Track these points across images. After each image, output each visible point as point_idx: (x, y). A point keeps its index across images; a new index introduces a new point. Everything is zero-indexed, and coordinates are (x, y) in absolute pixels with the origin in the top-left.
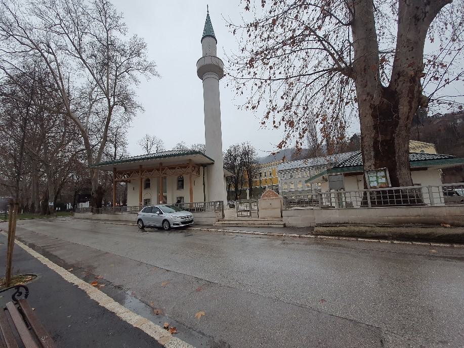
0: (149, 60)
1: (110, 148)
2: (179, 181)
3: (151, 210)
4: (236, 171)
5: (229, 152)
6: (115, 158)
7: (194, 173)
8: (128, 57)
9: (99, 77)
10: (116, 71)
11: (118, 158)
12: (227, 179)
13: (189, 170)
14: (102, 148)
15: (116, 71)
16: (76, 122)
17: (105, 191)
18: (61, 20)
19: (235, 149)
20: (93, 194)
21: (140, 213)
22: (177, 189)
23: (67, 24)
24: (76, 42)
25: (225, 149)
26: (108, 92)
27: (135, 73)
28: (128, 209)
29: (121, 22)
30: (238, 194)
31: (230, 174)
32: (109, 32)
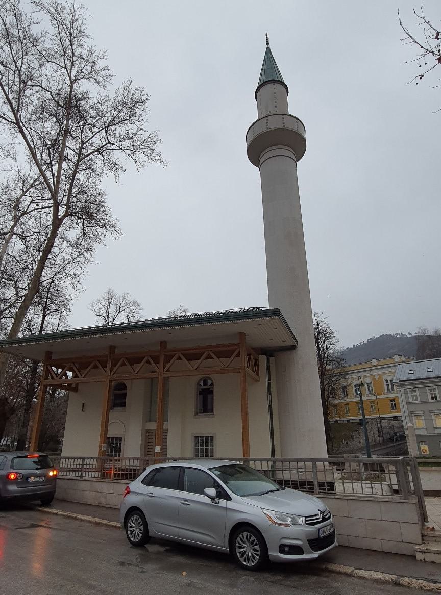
1: (34, 315)
21: (136, 485)
22: (196, 414)
27: (118, 156)
29: (101, 64)
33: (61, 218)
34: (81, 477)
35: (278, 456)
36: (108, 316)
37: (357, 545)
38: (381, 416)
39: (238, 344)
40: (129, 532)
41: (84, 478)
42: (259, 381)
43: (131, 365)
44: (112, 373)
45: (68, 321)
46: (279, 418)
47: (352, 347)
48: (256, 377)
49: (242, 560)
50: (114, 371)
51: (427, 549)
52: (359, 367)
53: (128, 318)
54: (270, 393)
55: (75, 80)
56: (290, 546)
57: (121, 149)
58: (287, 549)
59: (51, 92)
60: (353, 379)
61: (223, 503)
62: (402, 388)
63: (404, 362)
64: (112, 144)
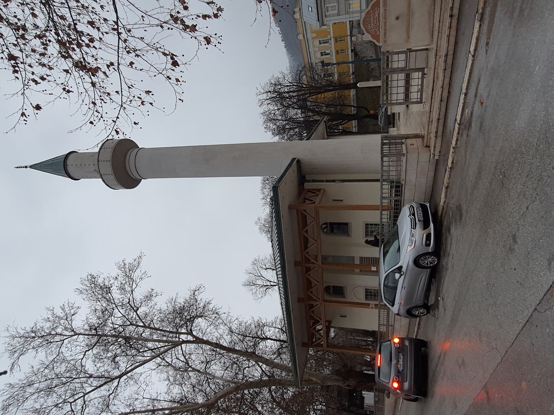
0: (115, 272)
2: (332, 231)
3: (391, 289)
4: (317, 118)
5: (281, 131)
6: (285, 342)
7: (317, 200)
8: (114, 306)
9: (148, 354)
10: (137, 326)
11: (283, 337)
12: (331, 133)
13: (309, 207)
14: (267, 362)
15: (137, 326)
16: (223, 396)
17: (345, 366)
18: (65, 401)
19: (271, 120)
20: (348, 386)
22: (349, 235)
23: (68, 394)
24: (95, 383)
25: (269, 138)
26: (171, 342)
27: (139, 295)
28: (383, 329)
29: (59, 312)
30: (366, 113)
31: (321, 128)
32: (78, 332)
33: (195, 338)
34: (392, 326)
35: (379, 177)
36: (265, 286)
37: (431, 184)
38: (349, 34)
39: (297, 211)
40: (421, 315)
41: (393, 324)
42: (324, 189)
43: (311, 287)
44: (319, 300)
45: (272, 321)
46: (353, 173)
47: (284, 42)
48: (322, 191)
49: (434, 264)
50: (316, 299)
51: (433, 154)
52: (305, 50)
53: (267, 269)
54: (334, 181)
55: (73, 331)
56: (427, 240)
57: (132, 291)
58: (428, 242)
59: (86, 351)
60: (316, 58)
61: (404, 269)
62: (325, 19)
63: (300, 9)
64: (129, 300)
